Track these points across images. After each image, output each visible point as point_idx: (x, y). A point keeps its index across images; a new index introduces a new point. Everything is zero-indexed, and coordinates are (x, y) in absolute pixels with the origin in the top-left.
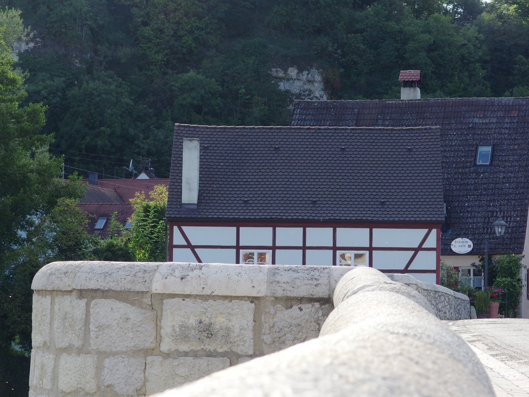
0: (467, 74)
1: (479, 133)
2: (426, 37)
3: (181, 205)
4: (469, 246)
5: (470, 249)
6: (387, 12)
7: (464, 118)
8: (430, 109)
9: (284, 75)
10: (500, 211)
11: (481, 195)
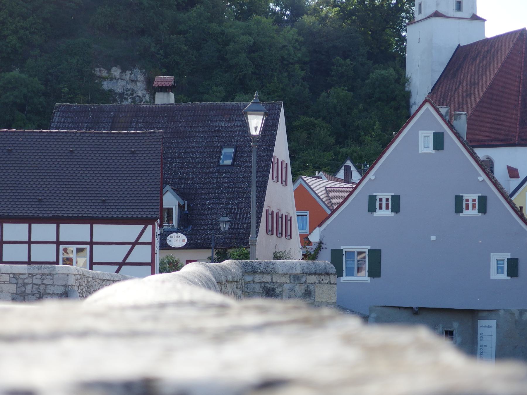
0: (286, 74)
1: (224, 135)
2: (246, 38)
4: (184, 241)
5: (184, 244)
6: (209, 14)
7: (211, 121)
8: (181, 113)
9: (107, 75)
10: (238, 208)
11: (222, 194)
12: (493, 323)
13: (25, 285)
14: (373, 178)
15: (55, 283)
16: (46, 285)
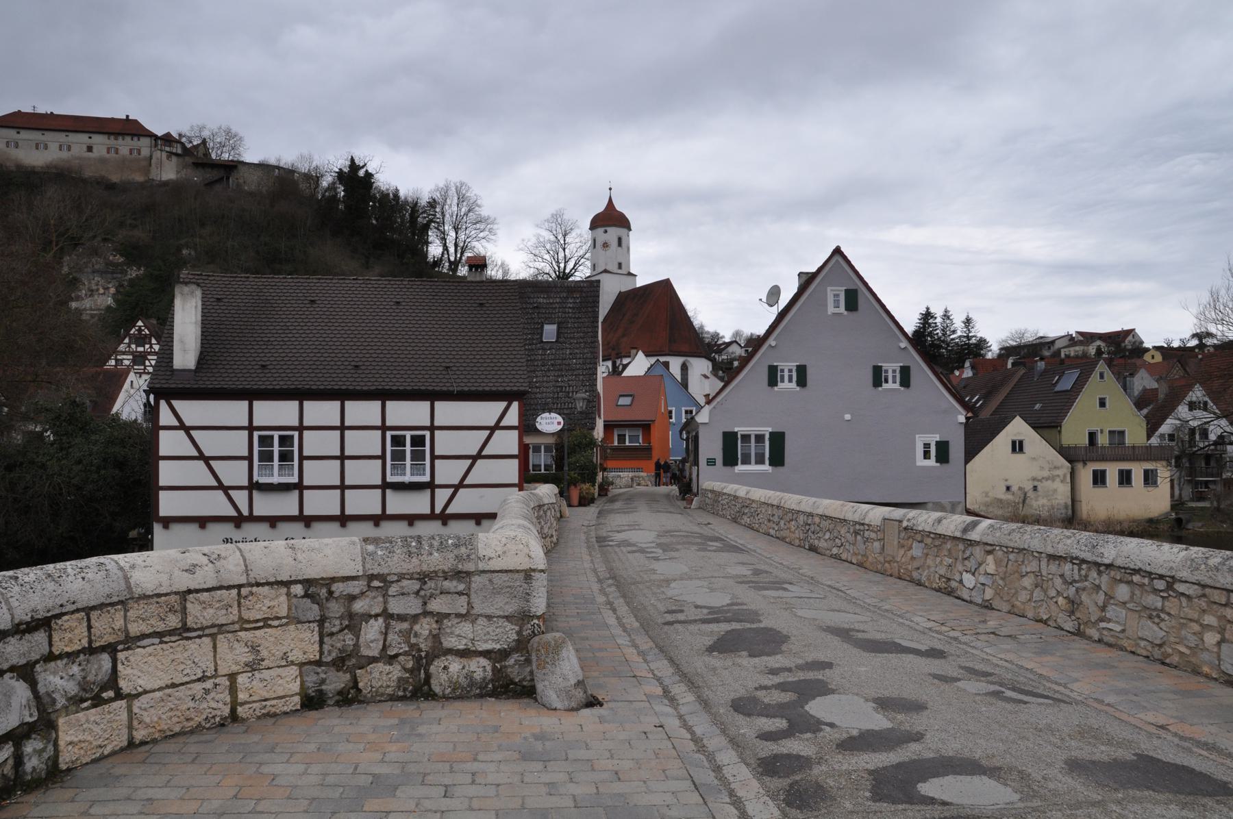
3: (173, 371)
4: (559, 423)
13: (354, 623)
14: (773, 344)
15: (478, 609)
16: (440, 617)
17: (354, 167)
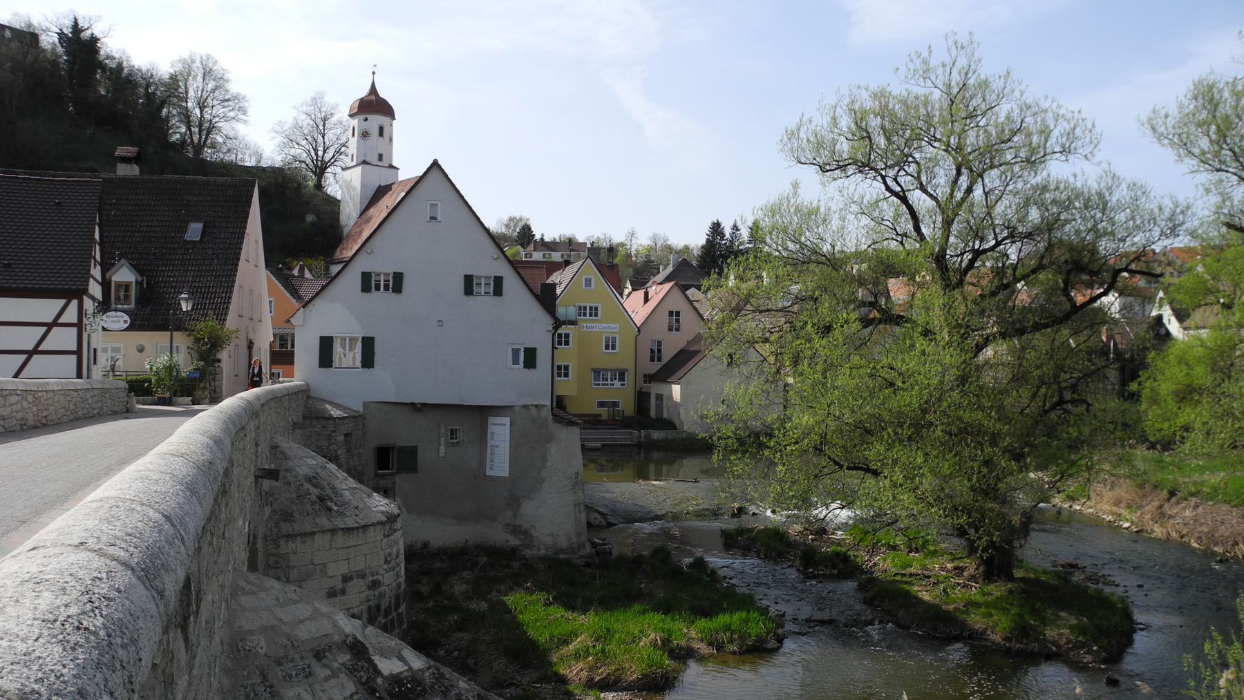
4: (125, 322)
12: (507, 420)
17: (76, 29)
